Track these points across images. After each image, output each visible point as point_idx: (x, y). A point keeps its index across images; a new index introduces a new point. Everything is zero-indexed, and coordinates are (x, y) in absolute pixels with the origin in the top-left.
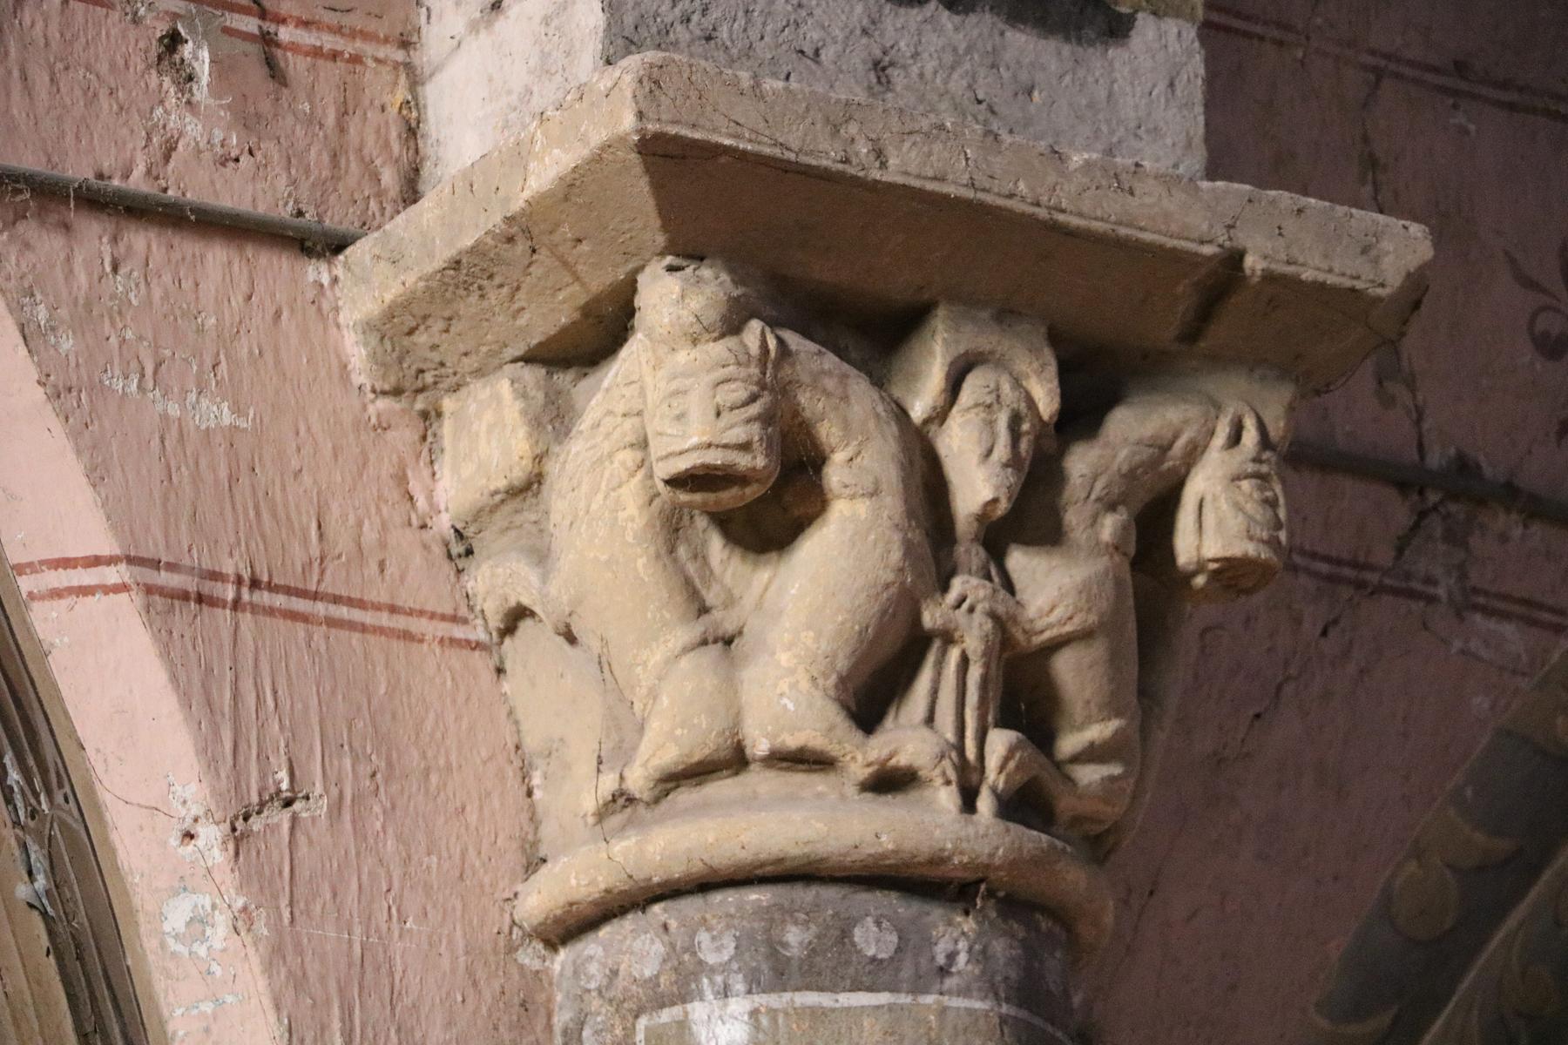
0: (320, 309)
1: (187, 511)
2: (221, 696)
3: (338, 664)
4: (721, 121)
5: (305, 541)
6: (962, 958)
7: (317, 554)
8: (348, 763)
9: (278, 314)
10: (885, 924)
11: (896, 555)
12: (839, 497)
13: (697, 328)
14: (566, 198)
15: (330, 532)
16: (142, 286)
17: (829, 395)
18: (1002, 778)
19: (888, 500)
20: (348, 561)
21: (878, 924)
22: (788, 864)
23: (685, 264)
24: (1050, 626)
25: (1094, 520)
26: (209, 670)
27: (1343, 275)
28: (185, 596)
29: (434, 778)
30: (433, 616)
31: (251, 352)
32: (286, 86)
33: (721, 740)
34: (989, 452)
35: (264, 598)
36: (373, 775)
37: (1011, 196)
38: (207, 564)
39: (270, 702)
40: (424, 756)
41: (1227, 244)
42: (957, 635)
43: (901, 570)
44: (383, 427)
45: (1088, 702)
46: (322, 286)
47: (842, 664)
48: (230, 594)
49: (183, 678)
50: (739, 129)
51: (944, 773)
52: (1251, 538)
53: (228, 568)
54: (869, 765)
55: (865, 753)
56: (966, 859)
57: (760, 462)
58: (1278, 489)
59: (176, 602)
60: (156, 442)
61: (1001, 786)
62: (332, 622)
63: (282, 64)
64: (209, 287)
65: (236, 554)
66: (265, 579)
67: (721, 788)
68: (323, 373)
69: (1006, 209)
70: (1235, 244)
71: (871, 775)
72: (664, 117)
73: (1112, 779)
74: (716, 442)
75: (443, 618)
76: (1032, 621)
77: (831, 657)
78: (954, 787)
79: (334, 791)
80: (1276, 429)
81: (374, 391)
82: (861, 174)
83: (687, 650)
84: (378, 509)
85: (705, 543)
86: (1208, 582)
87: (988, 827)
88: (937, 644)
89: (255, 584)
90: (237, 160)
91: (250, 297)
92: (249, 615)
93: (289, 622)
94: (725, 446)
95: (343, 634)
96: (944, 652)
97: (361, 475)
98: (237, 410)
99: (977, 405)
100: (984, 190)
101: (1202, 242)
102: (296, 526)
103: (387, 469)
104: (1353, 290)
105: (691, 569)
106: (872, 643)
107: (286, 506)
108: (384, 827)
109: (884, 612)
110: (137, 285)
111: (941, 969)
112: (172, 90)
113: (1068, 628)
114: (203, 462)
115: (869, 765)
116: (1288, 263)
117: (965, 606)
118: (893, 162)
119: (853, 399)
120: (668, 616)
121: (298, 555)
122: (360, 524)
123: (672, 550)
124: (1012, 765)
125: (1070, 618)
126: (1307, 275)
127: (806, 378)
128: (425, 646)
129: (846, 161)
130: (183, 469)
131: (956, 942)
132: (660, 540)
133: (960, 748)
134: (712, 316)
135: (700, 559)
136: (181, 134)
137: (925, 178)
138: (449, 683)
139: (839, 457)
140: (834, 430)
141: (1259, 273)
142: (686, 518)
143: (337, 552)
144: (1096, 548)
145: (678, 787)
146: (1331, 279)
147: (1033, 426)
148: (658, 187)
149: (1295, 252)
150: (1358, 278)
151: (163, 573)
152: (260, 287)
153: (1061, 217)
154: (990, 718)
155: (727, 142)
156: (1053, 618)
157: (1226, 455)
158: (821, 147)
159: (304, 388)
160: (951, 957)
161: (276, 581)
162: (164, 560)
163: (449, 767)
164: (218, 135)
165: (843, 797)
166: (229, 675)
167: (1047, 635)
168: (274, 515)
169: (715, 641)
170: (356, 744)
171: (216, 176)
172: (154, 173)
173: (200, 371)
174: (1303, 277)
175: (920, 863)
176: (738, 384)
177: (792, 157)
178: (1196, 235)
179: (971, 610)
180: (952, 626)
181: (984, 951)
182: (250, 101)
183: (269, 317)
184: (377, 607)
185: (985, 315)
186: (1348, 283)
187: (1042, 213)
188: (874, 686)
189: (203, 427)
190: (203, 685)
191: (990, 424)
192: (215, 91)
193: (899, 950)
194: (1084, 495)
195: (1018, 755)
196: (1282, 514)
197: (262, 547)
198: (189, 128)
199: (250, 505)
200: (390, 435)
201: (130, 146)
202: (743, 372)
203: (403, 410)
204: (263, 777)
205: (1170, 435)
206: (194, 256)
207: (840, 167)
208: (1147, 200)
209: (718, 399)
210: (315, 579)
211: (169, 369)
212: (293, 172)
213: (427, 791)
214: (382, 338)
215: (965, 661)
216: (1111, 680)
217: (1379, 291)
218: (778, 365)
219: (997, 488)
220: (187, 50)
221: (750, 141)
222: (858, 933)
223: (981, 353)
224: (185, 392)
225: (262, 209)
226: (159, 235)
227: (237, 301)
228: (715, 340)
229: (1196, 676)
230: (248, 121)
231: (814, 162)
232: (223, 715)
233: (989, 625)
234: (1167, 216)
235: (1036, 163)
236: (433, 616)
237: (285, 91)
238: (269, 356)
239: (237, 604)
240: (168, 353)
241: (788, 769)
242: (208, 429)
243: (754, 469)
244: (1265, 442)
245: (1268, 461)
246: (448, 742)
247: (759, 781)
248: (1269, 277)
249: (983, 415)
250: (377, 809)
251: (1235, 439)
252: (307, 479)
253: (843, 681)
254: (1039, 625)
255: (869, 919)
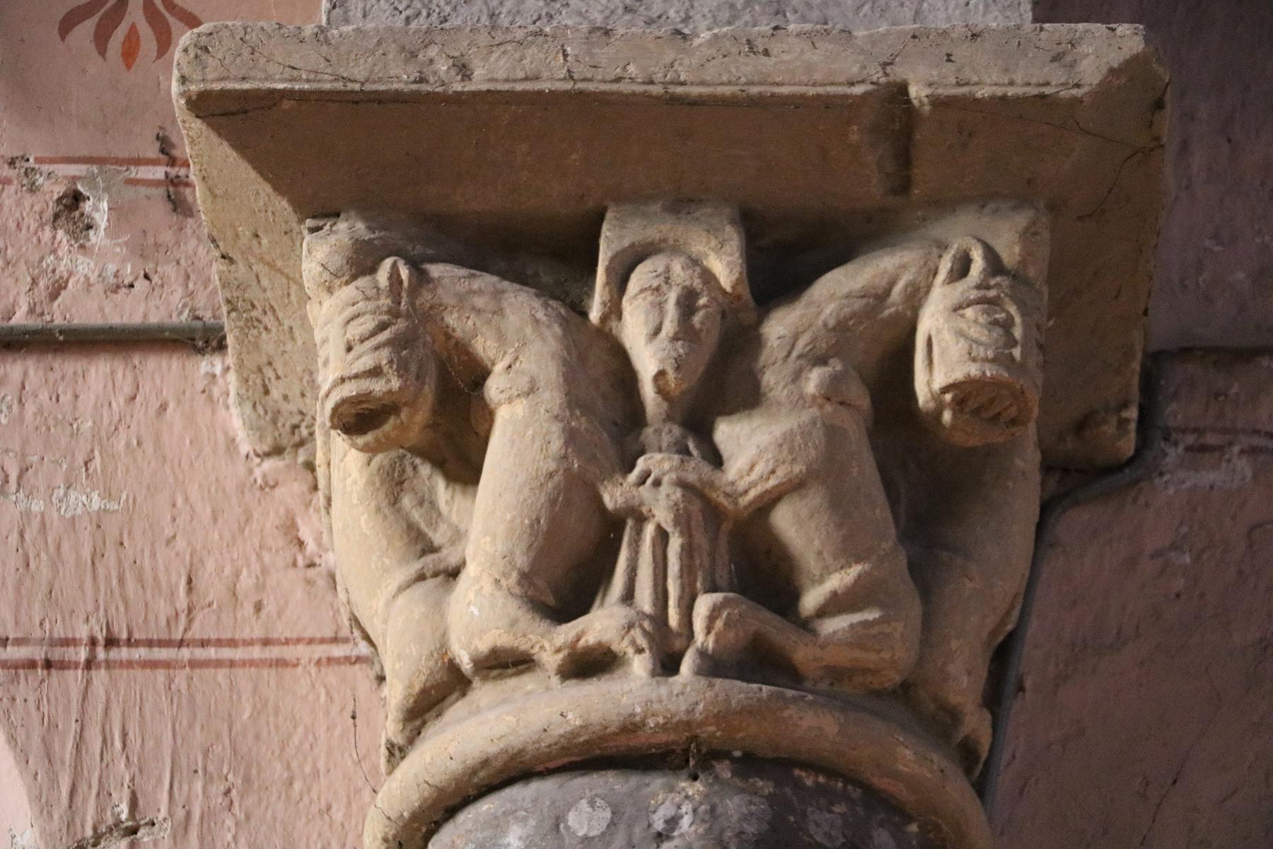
0: (210, 398)
1: (44, 588)
2: (63, 745)
3: (199, 697)
4: (273, 69)
5: (173, 594)
6: (685, 822)
7: (185, 606)
8: (198, 786)
9: (163, 407)
10: (599, 802)
11: (556, 445)
12: (500, 404)
13: (326, 276)
14: (215, 196)
15: (200, 585)
16: (15, 408)
17: (478, 311)
18: (711, 638)
19: (546, 395)
20: (219, 607)
21: (592, 804)
22: (498, 764)
23: (321, 223)
24: (753, 484)
25: (797, 376)
26: (53, 726)
27: (1029, 84)
28: (32, 665)
29: (297, 786)
30: (311, 641)
31: (128, 445)
32: (191, 216)
33: (432, 663)
34: (657, 331)
35: (124, 653)
36: (228, 792)
37: (618, 80)
38: (59, 632)
39: (118, 744)
40: (288, 767)
41: (883, 80)
42: (644, 510)
43: (565, 457)
44: (269, 485)
45: (820, 553)
46: (214, 376)
47: (522, 561)
48: (82, 654)
49: (21, 735)
50: (295, 73)
51: (633, 642)
52: (974, 360)
53: (83, 632)
54: (558, 651)
55: (551, 641)
56: (661, 721)
57: (395, 384)
58: (1013, 309)
59: (21, 672)
60: (14, 537)
61: (710, 645)
62: (194, 664)
63: (190, 199)
64: (88, 399)
65: (93, 620)
66: (124, 636)
67: (457, 710)
68: (207, 449)
69: (613, 93)
70: (891, 78)
71: (563, 660)
72: (210, 77)
73: (866, 624)
74: (346, 374)
75: (322, 641)
76: (733, 483)
77: (508, 557)
78: (647, 654)
79: (180, 813)
80: (1010, 253)
81: (258, 455)
82: (440, 89)
83: (402, 589)
84: (259, 556)
85: (432, 490)
86: (954, 416)
87: (685, 685)
88: (630, 523)
89: (111, 642)
90: (132, 286)
91: (134, 398)
92: (103, 671)
93: (148, 671)
94: (356, 376)
95: (208, 672)
96: (639, 531)
97: (242, 531)
98: (108, 495)
99: (642, 291)
100: (584, 80)
101: (852, 84)
102: (164, 584)
103: (272, 521)
104: (1043, 97)
105: (417, 516)
106: (549, 534)
107: (154, 569)
108: (235, 838)
109: (553, 502)
110: (10, 407)
111: (659, 835)
112: (65, 240)
113: (772, 482)
114: (66, 546)
115: (558, 651)
116: (958, 84)
117: (649, 481)
118: (479, 73)
119: (508, 311)
120: (387, 561)
121: (162, 609)
122: (237, 574)
123: (395, 502)
124: (719, 624)
125: (773, 472)
126: (982, 92)
127: (449, 300)
128: (300, 669)
129: (422, 80)
130: (43, 555)
131: (679, 807)
132: (381, 495)
133: (660, 618)
134: (337, 261)
135: (426, 504)
136: (71, 274)
137: (515, 81)
138: (323, 698)
139: (499, 368)
140: (488, 343)
141: (926, 100)
142: (409, 470)
143: (207, 601)
144: (801, 401)
145: (424, 723)
146: (1011, 92)
147: (712, 299)
148: (241, 147)
149: (967, 74)
150: (1048, 84)
151: (9, 648)
152: (146, 388)
153: (680, 90)
154: (699, 585)
155: (280, 86)
156: (754, 476)
157: (948, 289)
158: (392, 73)
159: (185, 466)
160: (673, 822)
161: (136, 636)
162: (11, 637)
163: (316, 773)
164: (111, 268)
165: (548, 689)
166: (74, 727)
167: (753, 494)
168: (140, 580)
169: (435, 575)
170: (211, 768)
171: (105, 303)
172: (38, 310)
173: (71, 468)
174: (979, 95)
175: (615, 734)
176: (368, 316)
177: (357, 87)
178: (842, 79)
179: (657, 483)
180: (636, 502)
181: (713, 810)
182: (150, 234)
183: (152, 412)
184: (248, 643)
185: (656, 207)
186: (1034, 91)
187: (656, 90)
188: (568, 573)
189: (68, 515)
190: (44, 740)
191: (660, 307)
192: (112, 232)
193: (612, 824)
194: (784, 353)
195: (725, 614)
196: (1018, 332)
197: (122, 609)
198: (80, 268)
199: (114, 574)
200: (278, 491)
201: (13, 293)
202: (371, 305)
203: (287, 466)
204: (100, 810)
205: (884, 283)
206: (75, 373)
207: (414, 87)
208: (786, 57)
209: (348, 336)
210: (181, 628)
211: (36, 473)
212: (191, 285)
213: (288, 798)
214: (254, 405)
215: (662, 537)
216: (839, 526)
217: (1075, 92)
218: (414, 291)
219: (662, 361)
220: (87, 207)
221: (308, 81)
222: (572, 818)
223: (652, 243)
224: (51, 489)
225: (154, 319)
226: (39, 361)
227: (119, 402)
228: (347, 283)
229: (1240, 572)
230: (145, 250)
231: (382, 88)
232: (63, 763)
233: (678, 494)
234: (809, 68)
235: (652, 46)
236: (311, 641)
237: (190, 220)
238: (149, 446)
239: (90, 664)
240: (35, 458)
241: (500, 677)
242: (73, 518)
243: (390, 392)
244: (995, 265)
245: (997, 285)
246: (316, 751)
247: (483, 693)
248: (939, 103)
249: (650, 298)
250: (230, 822)
251: (962, 268)
252: (180, 543)
253: (526, 578)
254: (742, 485)
255: (584, 801)
